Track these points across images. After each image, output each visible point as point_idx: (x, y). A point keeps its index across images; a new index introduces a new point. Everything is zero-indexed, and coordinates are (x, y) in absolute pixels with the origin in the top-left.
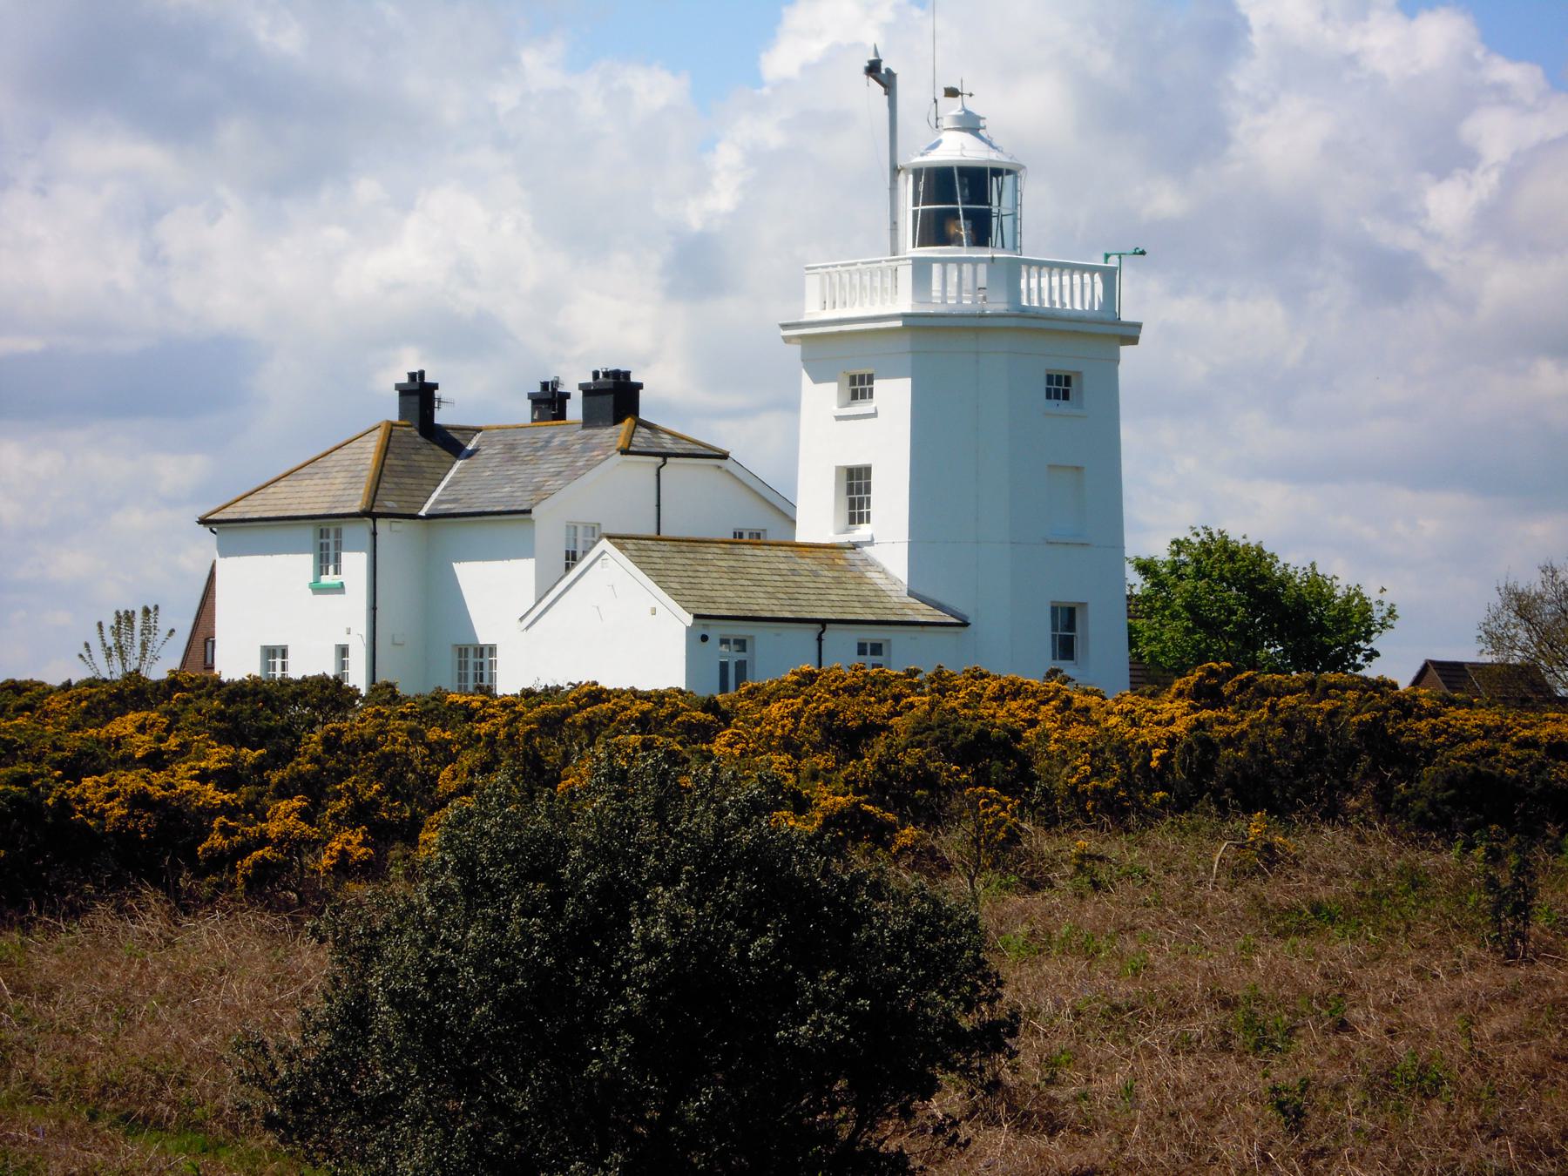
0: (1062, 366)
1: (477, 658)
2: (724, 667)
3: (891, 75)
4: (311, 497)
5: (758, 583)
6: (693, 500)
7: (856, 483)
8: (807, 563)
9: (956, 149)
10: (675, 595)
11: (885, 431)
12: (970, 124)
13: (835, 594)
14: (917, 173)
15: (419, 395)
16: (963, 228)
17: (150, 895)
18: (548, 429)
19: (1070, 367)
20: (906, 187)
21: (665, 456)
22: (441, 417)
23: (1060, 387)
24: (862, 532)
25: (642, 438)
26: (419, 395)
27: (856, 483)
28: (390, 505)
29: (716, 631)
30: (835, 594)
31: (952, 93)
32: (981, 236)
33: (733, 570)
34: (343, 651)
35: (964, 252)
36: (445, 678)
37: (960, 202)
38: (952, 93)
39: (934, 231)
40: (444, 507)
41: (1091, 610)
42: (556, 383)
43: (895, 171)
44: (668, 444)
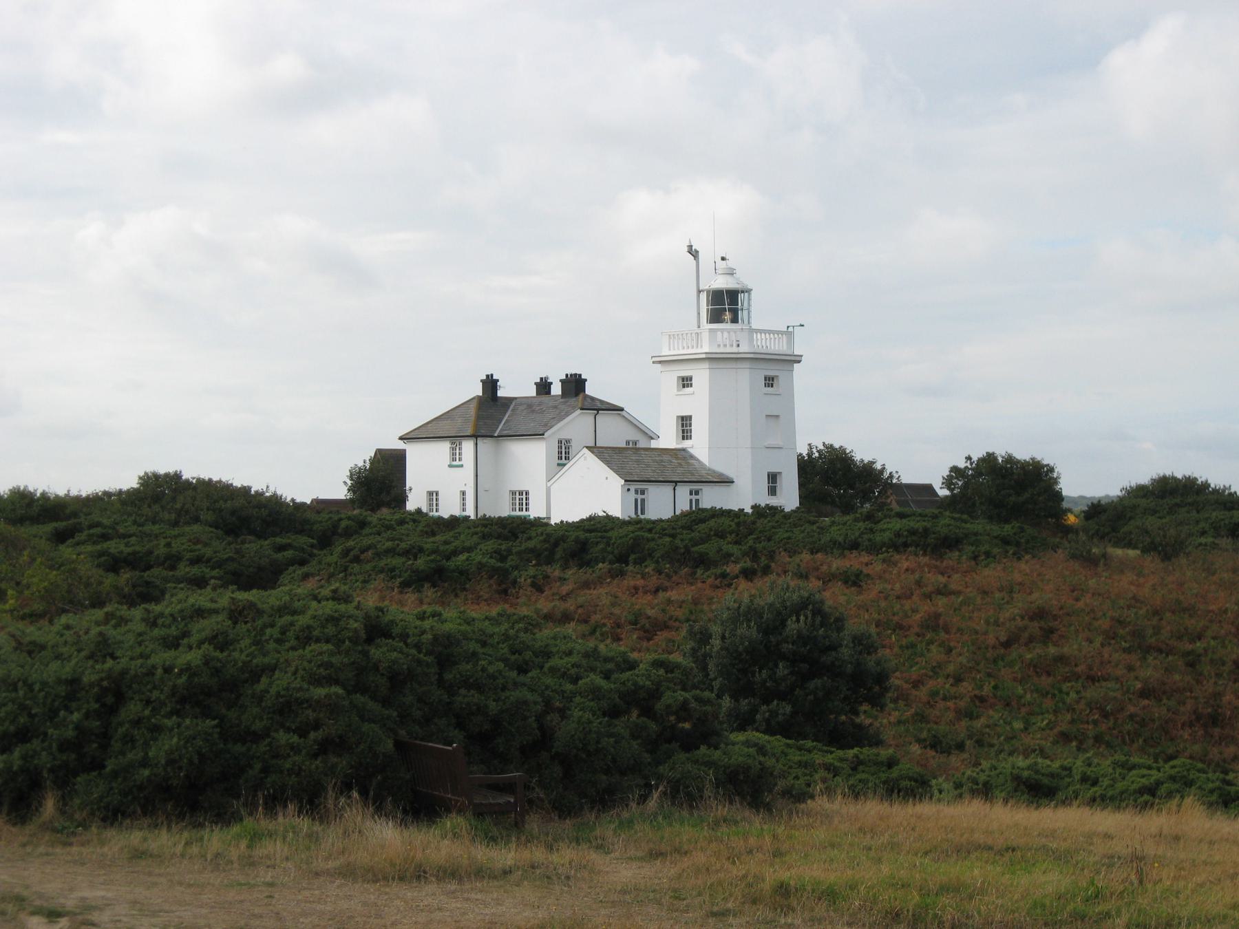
0: (771, 373)
1: (522, 497)
2: (636, 500)
3: (697, 252)
4: (447, 428)
5: (648, 466)
6: (613, 433)
7: (685, 424)
8: (666, 458)
9: (722, 283)
10: (616, 472)
11: (697, 403)
12: (731, 272)
13: (680, 470)
14: (708, 292)
15: (490, 384)
16: (728, 316)
17: (426, 585)
18: (544, 398)
19: (773, 369)
20: (704, 297)
21: (598, 410)
22: (500, 393)
23: (770, 381)
24: (686, 444)
25: (587, 405)
26: (490, 384)
27: (685, 424)
28: (483, 432)
29: (633, 487)
30: (680, 470)
31: (723, 259)
32: (735, 320)
33: (637, 461)
34: (773, 478)
35: (729, 326)
36: (503, 509)
37: (725, 305)
38: (723, 259)
39: (716, 317)
40: (505, 433)
41: (783, 475)
42: (546, 378)
43: (699, 292)
44: (599, 405)
